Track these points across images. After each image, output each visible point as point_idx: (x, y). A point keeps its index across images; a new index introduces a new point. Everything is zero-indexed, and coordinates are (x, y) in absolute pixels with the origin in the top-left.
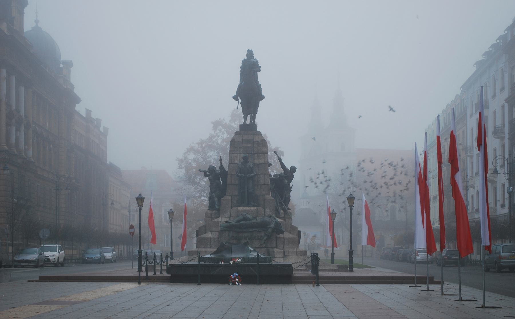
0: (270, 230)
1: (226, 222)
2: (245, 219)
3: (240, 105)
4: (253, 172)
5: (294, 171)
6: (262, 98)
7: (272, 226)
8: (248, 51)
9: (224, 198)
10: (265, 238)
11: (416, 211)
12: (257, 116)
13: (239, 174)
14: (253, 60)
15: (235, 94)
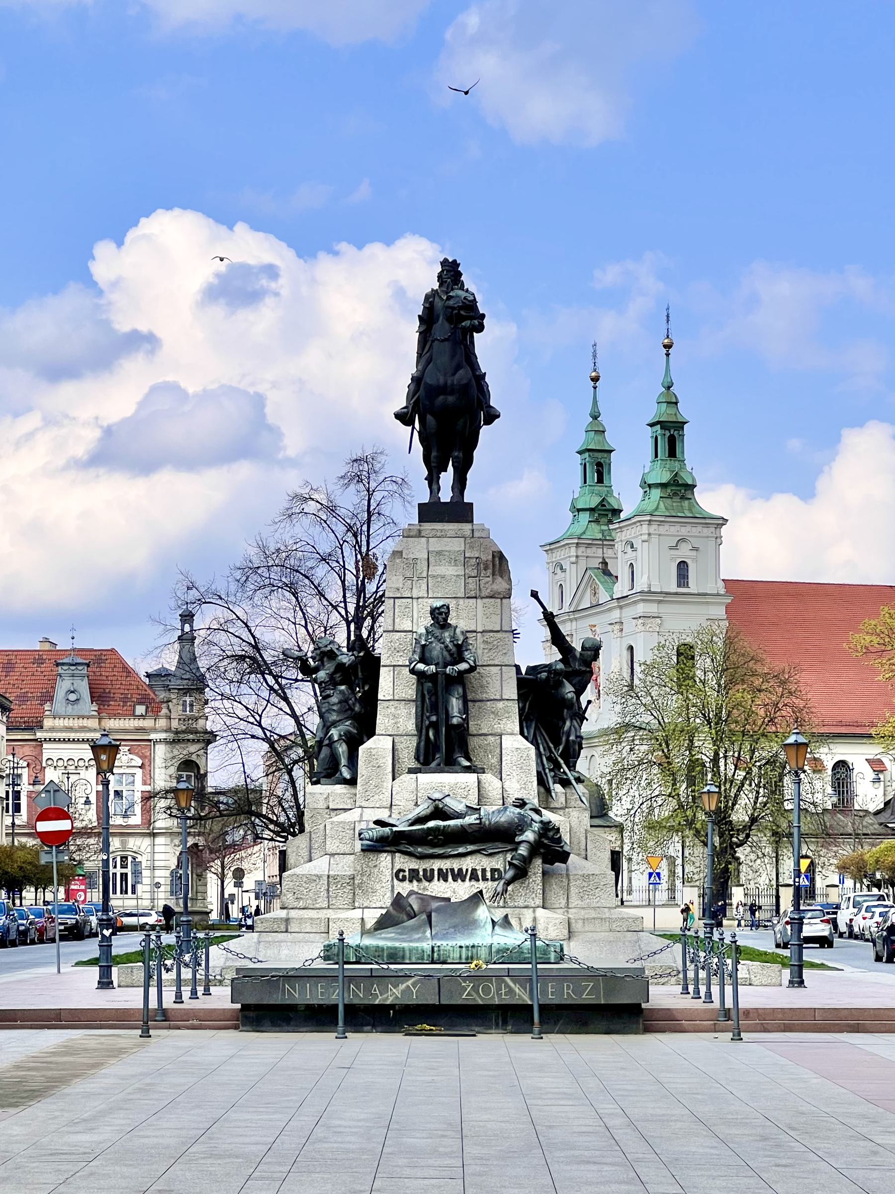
0: (523, 850)
1: (378, 823)
2: (439, 813)
3: (416, 434)
4: (463, 660)
5: (596, 657)
6: (492, 417)
7: (529, 836)
8: (445, 263)
9: (369, 744)
10: (510, 874)
11: (675, 1032)
12: (471, 475)
13: (421, 666)
14: (462, 294)
15: (400, 402)
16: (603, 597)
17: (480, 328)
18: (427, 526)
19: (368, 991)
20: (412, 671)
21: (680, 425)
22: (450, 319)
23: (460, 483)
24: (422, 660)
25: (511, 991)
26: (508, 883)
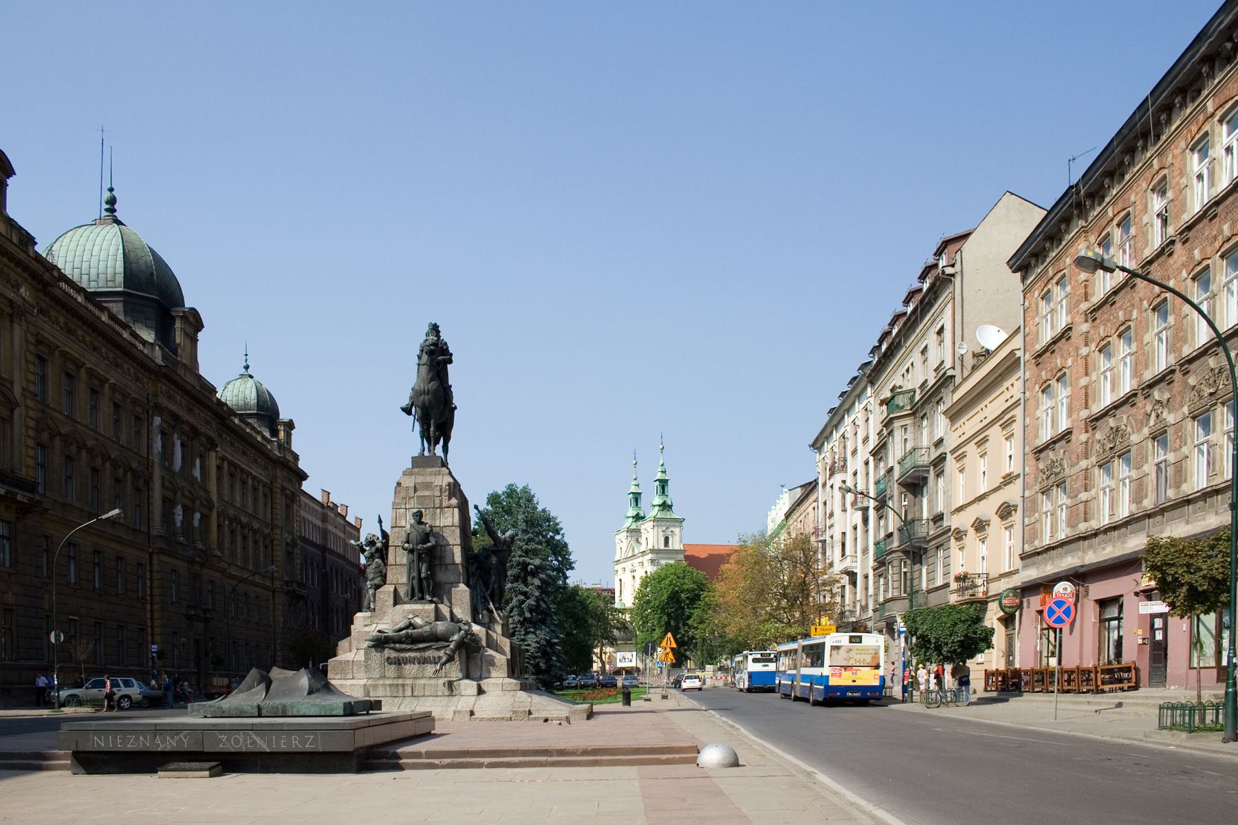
2: (411, 625)
15: (406, 402)
16: (636, 552)
17: (451, 362)
18: (416, 470)
19: (124, 740)
20: (404, 549)
21: (666, 481)
22: (437, 357)
23: (445, 449)
24: (408, 542)
25: (254, 743)
26: (444, 664)
